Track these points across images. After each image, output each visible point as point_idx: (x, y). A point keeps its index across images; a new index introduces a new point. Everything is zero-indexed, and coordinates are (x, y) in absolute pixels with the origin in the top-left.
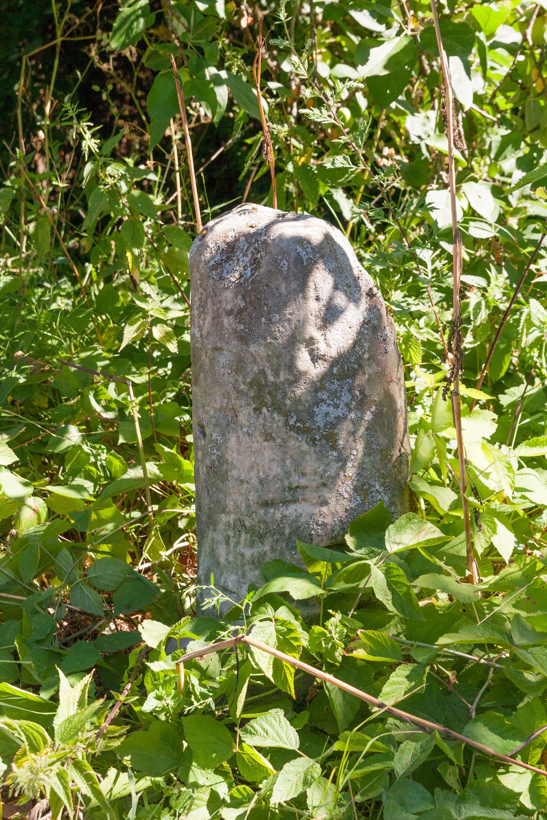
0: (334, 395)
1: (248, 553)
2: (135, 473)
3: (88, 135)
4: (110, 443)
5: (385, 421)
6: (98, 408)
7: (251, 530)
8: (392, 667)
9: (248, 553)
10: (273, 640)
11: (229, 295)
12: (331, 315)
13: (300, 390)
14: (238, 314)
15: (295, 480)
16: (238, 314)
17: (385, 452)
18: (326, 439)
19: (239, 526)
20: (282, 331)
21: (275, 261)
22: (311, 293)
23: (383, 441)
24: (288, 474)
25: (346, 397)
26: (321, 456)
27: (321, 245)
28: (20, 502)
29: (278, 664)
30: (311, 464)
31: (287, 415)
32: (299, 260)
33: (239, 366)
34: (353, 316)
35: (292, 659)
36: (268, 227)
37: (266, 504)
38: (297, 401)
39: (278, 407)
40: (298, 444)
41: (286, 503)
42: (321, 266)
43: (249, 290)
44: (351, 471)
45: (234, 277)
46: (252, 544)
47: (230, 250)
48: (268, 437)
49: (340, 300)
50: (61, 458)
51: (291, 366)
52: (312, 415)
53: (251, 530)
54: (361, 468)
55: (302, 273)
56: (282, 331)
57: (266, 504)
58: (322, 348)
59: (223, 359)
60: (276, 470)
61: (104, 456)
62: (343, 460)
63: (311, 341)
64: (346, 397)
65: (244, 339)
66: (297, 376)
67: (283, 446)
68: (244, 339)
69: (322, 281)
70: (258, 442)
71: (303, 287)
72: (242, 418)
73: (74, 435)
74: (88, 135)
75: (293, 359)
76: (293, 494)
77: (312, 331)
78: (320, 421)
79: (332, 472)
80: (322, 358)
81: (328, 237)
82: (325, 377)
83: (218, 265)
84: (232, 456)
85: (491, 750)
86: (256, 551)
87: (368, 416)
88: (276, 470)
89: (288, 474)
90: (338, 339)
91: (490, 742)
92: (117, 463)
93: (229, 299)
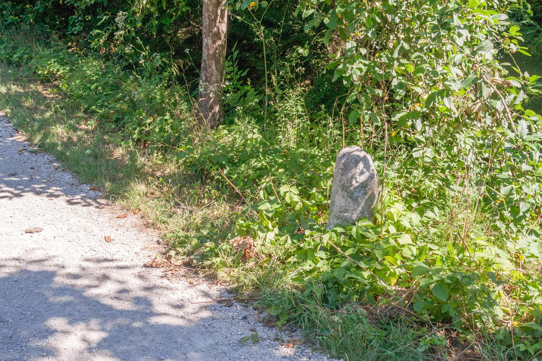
0: (359, 191)
1: (336, 222)
2: (326, 202)
3: (331, 123)
4: (322, 193)
5: (372, 198)
6: (323, 185)
7: (337, 217)
8: (349, 248)
9: (336, 222)
10: (328, 238)
11: (341, 165)
12: (362, 173)
13: (352, 188)
14: (342, 169)
15: (347, 208)
16: (342, 169)
17: (370, 206)
18: (356, 200)
19: (335, 216)
20: (350, 175)
21: (351, 160)
22: (358, 168)
23: (370, 203)
24: (346, 206)
25: (362, 192)
26: (354, 203)
27: (362, 158)
28: (297, 203)
29: (328, 243)
30: (351, 205)
31: (348, 193)
32: (356, 160)
33: (340, 181)
34: (367, 174)
35: (330, 242)
36: (353, 152)
37: (341, 212)
38: (351, 191)
39: (346, 191)
40: (349, 200)
41: (345, 212)
42: (361, 162)
43: (345, 164)
44: (360, 208)
45: (343, 161)
46: (337, 220)
47: (344, 155)
48: (343, 197)
49: (365, 170)
50: (310, 195)
51: (351, 183)
52: (353, 194)
53: (337, 217)
54: (363, 207)
55: (357, 163)
56: (350, 175)
57: (341, 212)
58: (358, 180)
59: (338, 178)
60: (344, 205)
61: (320, 196)
62: (359, 205)
63: (356, 178)
64: (362, 192)
65: (342, 175)
66: (351, 185)
67: (346, 199)
68: (342, 175)
69: (361, 166)
70: (341, 198)
71: (356, 166)
72: (339, 192)
73: (314, 190)
74: (331, 123)
75: (352, 181)
76: (346, 211)
77: (357, 176)
78: (355, 196)
79: (356, 207)
80: (358, 182)
81: (365, 156)
82: (358, 187)
83: (341, 158)
84: (336, 200)
85: (362, 266)
86: (337, 221)
87: (367, 197)
88: (344, 205)
89: (346, 206)
90: (362, 179)
91: (362, 265)
92: (323, 199)
93: (341, 166)
